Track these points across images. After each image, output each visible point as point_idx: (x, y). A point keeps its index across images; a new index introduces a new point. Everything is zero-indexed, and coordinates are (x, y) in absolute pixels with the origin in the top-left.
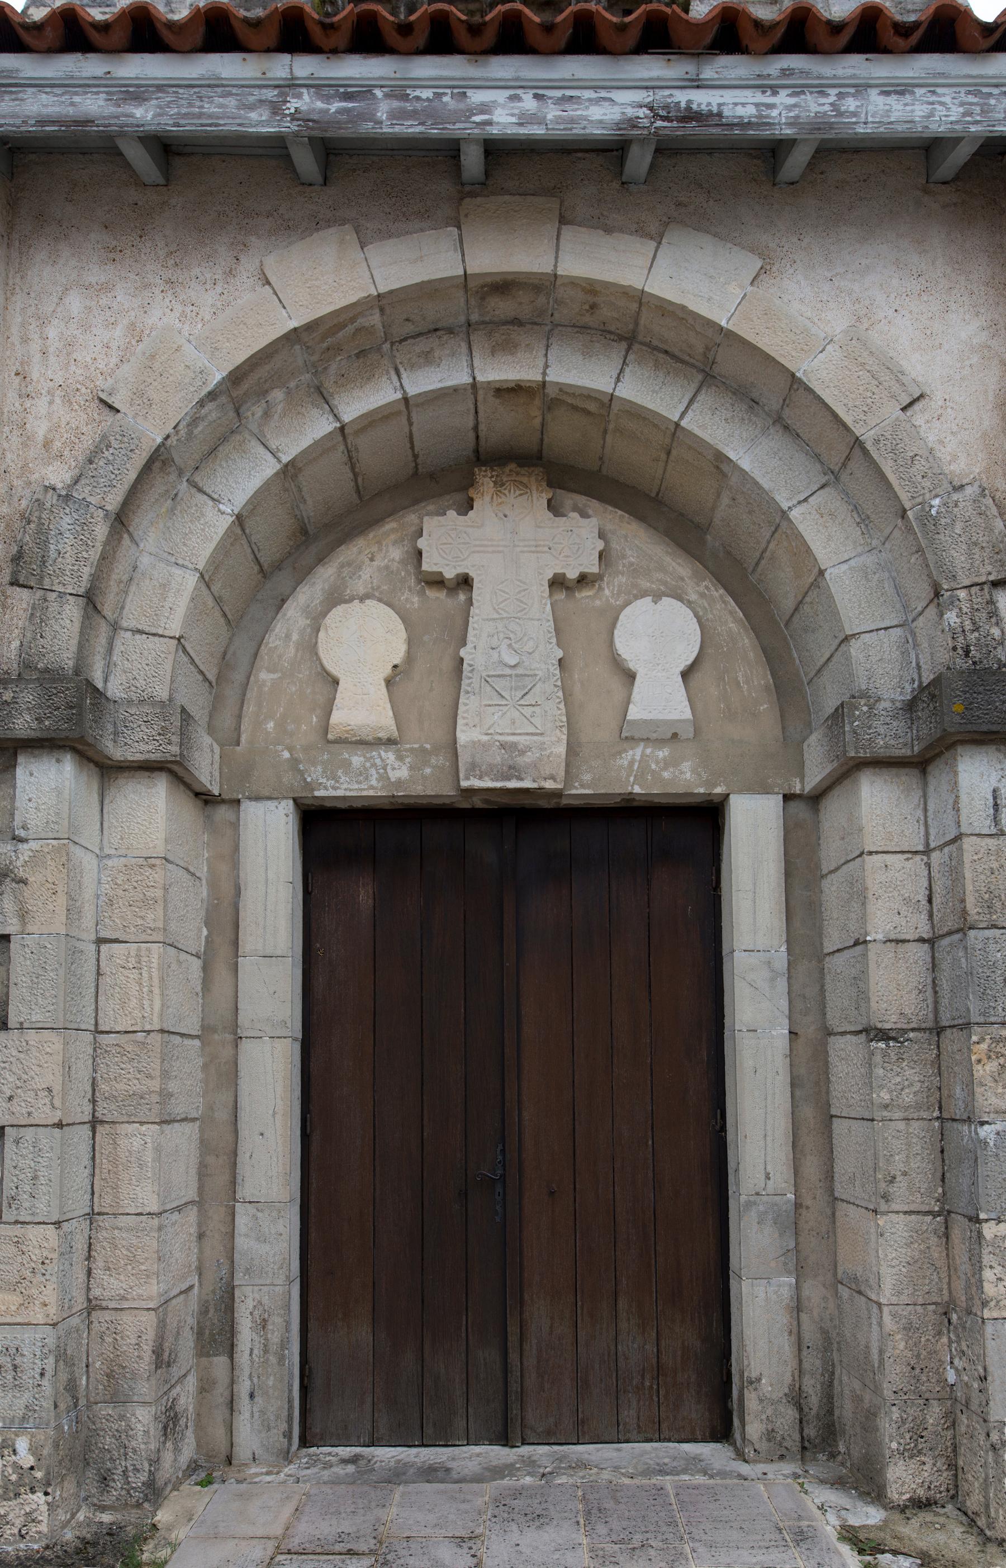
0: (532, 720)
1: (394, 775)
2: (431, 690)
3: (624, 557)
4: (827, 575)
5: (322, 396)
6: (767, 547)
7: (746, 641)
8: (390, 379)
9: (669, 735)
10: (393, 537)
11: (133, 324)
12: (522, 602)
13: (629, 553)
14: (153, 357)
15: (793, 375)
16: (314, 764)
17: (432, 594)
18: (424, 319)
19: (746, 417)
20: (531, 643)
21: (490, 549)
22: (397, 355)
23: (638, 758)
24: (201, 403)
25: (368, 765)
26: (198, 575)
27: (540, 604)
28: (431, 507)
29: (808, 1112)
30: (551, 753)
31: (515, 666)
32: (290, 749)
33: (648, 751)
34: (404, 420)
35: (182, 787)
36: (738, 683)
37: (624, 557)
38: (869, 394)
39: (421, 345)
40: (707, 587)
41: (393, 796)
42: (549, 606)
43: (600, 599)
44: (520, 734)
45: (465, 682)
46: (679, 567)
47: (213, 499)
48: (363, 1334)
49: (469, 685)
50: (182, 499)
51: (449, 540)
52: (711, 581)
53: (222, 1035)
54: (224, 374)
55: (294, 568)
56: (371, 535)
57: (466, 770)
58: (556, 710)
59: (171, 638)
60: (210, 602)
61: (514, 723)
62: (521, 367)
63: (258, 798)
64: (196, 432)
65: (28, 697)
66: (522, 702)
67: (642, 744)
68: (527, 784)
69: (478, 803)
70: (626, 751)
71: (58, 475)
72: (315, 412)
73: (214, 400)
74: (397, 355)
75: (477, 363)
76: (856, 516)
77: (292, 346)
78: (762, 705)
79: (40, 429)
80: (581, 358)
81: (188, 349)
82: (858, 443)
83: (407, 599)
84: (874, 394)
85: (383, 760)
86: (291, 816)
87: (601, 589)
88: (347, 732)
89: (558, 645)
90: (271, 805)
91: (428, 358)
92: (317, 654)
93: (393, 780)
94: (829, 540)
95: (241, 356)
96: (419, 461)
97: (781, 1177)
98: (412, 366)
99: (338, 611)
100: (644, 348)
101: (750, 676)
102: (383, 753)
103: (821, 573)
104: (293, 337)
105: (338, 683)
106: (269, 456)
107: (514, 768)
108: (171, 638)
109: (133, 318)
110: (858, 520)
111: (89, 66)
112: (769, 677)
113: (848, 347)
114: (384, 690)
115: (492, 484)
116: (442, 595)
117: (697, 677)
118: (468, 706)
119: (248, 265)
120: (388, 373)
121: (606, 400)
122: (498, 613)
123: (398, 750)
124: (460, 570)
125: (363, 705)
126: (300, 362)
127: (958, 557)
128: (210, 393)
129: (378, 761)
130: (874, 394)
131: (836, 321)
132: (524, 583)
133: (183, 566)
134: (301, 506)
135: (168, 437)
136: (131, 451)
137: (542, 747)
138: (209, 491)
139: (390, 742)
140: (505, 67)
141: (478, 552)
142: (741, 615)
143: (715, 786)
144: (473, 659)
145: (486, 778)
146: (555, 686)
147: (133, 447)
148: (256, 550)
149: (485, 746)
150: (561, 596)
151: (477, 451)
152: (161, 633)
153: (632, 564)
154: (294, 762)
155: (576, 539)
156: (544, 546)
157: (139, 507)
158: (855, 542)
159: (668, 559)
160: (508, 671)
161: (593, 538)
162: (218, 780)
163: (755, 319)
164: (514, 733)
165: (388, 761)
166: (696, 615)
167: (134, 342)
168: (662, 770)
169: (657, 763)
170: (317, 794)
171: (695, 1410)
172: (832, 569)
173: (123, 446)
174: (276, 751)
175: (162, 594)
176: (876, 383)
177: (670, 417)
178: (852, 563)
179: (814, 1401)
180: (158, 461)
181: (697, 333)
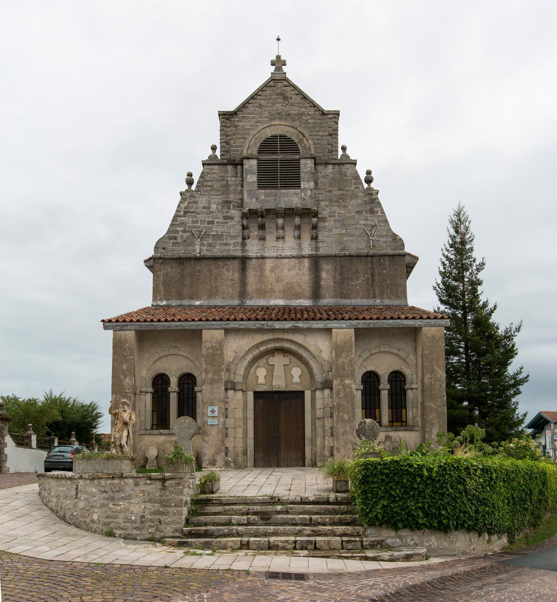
7: (307, 372)
29: (313, 428)
46: (299, 363)
48: (262, 454)
53: (245, 419)
58: (284, 381)
65: (229, 384)
71: (231, 360)
79: (229, 355)
91: (269, 343)
97: (310, 435)
101: (307, 376)
102: (345, 568)
111: (237, 322)
118: (274, 380)
119: (250, 336)
125: (261, 380)
127: (325, 369)
131: (313, 343)
140: (277, 322)
155: (286, 360)
164: (279, 384)
171: (301, 463)
179: (313, 461)
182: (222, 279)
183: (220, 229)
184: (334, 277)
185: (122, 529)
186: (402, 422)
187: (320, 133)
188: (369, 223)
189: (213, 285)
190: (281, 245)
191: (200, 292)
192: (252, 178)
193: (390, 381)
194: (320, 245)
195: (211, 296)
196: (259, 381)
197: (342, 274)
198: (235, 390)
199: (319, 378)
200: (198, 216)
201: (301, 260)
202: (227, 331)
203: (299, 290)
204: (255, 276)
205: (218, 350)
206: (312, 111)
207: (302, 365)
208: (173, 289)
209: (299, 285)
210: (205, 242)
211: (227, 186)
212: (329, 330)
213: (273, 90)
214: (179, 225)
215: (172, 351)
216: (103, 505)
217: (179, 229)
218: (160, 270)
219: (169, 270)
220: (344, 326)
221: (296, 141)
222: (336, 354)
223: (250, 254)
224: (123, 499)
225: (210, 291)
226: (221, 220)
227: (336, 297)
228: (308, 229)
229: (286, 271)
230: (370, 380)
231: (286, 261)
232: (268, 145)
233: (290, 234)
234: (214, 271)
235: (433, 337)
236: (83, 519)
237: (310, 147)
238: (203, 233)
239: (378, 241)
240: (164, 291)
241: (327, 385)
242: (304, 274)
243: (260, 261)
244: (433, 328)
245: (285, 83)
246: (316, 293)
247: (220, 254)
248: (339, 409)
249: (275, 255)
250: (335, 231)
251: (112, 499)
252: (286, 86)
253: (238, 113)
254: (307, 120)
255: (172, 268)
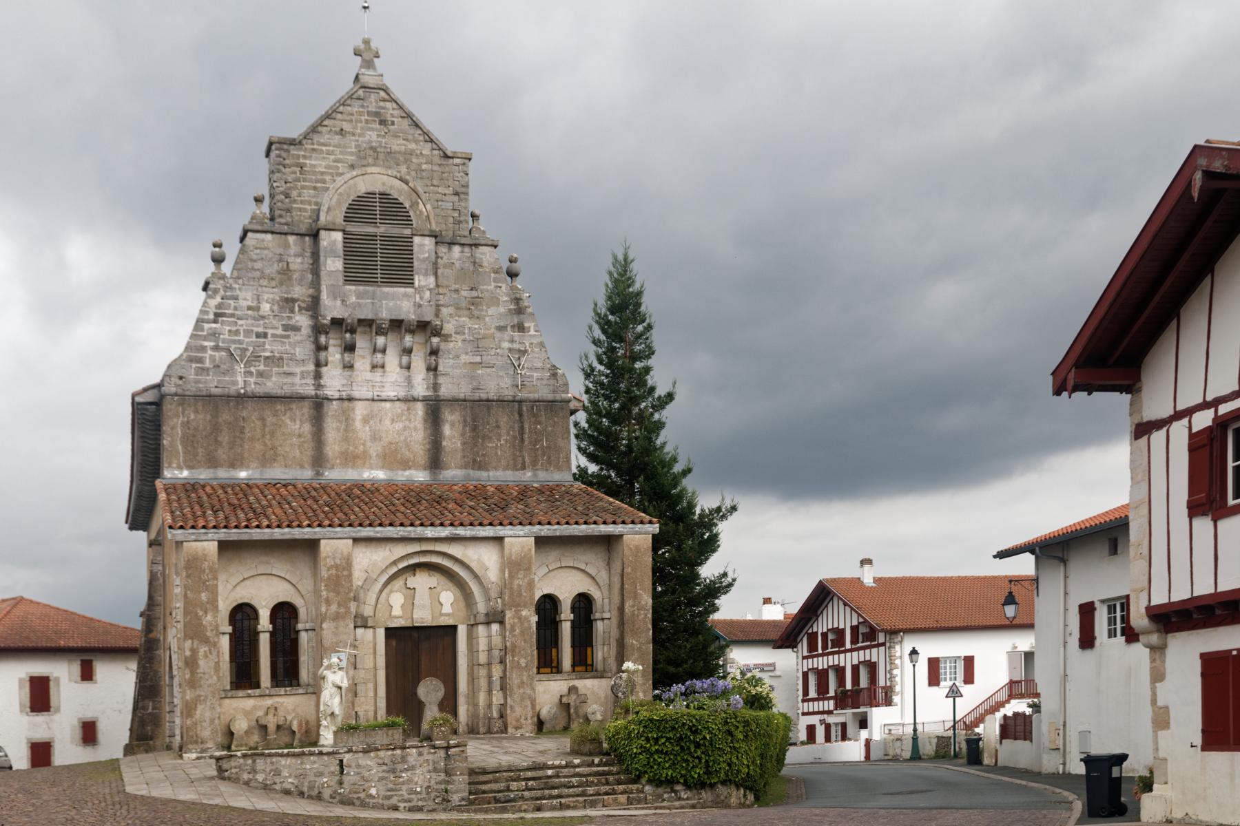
27: (427, 592)
46: (450, 585)
71: (360, 583)
101: (462, 604)
125: (397, 611)
164: (423, 616)
182: (284, 434)
183: (277, 348)
184: (463, 435)
185: (406, 801)
186: (586, 665)
187: (440, 190)
188: (516, 346)
189: (269, 443)
190: (378, 379)
191: (246, 455)
192: (333, 265)
193: (573, 609)
194: (441, 380)
195: (267, 460)
196: (395, 613)
197: (474, 429)
198: (365, 627)
199: (482, 607)
200: (240, 322)
201: (411, 404)
202: (356, 540)
203: (408, 455)
204: (338, 429)
205: (344, 569)
206: (426, 149)
207: (454, 588)
208: (200, 450)
209: (407, 446)
210: (252, 369)
211: (286, 272)
212: (499, 540)
213: (362, 106)
214: (205, 338)
215: (261, 570)
216: (381, 779)
217: (206, 343)
218: (177, 416)
219: (192, 416)
220: (521, 533)
221: (407, 205)
222: (510, 573)
223: (330, 392)
224: (406, 770)
225: (264, 455)
226: (280, 332)
227: (465, 467)
228: (421, 354)
229: (387, 422)
230: (548, 606)
231: (388, 405)
232: (359, 209)
233: (392, 359)
234: (270, 419)
235: (637, 548)
236: (356, 796)
237: (428, 216)
238: (248, 354)
239: (530, 377)
240: (184, 453)
241: (495, 617)
242: (415, 429)
243: (346, 403)
244: (637, 536)
245: (382, 94)
246: (435, 461)
247: (279, 392)
248: (513, 651)
249: (369, 395)
250: (465, 358)
251: (393, 771)
252: (384, 100)
253: (304, 142)
254: (420, 164)
255: (196, 412)
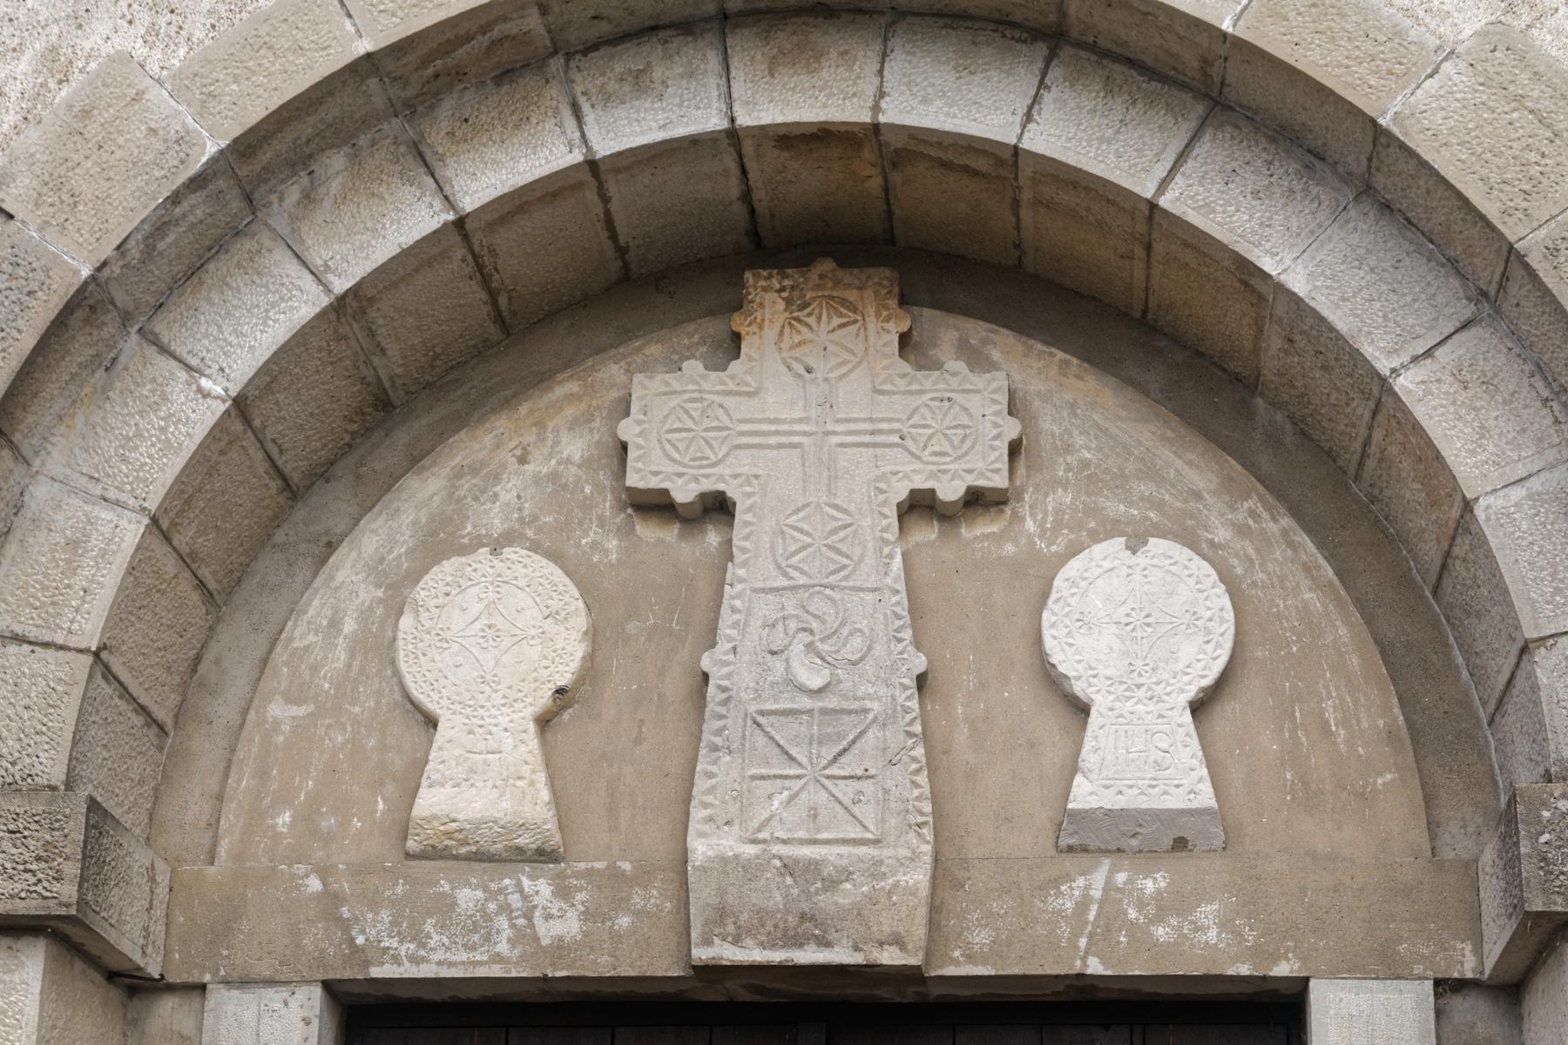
0: (856, 810)
1: (547, 931)
2: (638, 741)
3: (1068, 449)
4: (1479, 511)
5: (423, 159)
6: (1370, 436)
8: (560, 125)
9: (1168, 842)
10: (570, 412)
11: (54, 50)
12: (839, 552)
13: (1080, 440)
14: (87, 113)
15: (1373, 122)
16: (374, 906)
17: (650, 532)
18: (632, 13)
19: (1298, 187)
20: (857, 641)
21: (772, 440)
22: (578, 78)
23: (1097, 894)
24: (175, 198)
25: (492, 907)
26: (146, 521)
27: (881, 559)
28: (654, 350)
30: (896, 884)
31: (821, 691)
32: (324, 872)
33: (1121, 878)
34: (591, 196)
35: (79, 965)
36: (1326, 723)
37: (1068, 449)
38: (1533, 157)
39: (627, 60)
40: (1252, 513)
41: (545, 979)
42: (898, 558)
43: (1015, 542)
44: (828, 842)
45: (710, 725)
46: (1192, 471)
47: (189, 367)
49: (719, 732)
50: (126, 369)
51: (686, 411)
52: (1261, 499)
54: (223, 144)
55: (358, 477)
56: (523, 409)
57: (706, 924)
58: (909, 787)
59: (80, 651)
60: (170, 566)
61: (815, 816)
62: (829, 96)
63: (245, 982)
64: (161, 246)
66: (834, 770)
67: (1106, 863)
68: (840, 955)
69: (737, 990)
70: (1069, 878)
72: (406, 193)
73: (201, 187)
74: (578, 78)
75: (738, 89)
76: (1540, 384)
77: (363, 81)
78: (1380, 774)
80: (952, 76)
81: (159, 96)
82: (1512, 256)
83: (594, 544)
84: (1543, 155)
85: (525, 898)
86: (315, 1023)
87: (1017, 518)
88: (449, 835)
89: (918, 644)
90: (274, 997)
92: (393, 663)
93: (545, 942)
94: (1482, 436)
95: (255, 113)
96: (631, 256)
98: (607, 99)
99: (447, 569)
100: (1083, 53)
101: (1351, 707)
102: (526, 882)
103: (1468, 506)
104: (368, 64)
105: (435, 726)
106: (307, 281)
107: (812, 918)
108: (80, 651)
109: (54, 38)
110: (1546, 393)
112: (1397, 710)
113: (1488, 65)
114: (533, 743)
115: (781, 305)
116: (669, 534)
117: (1226, 714)
118: (718, 775)
120: (557, 111)
121: (1007, 155)
122: (786, 575)
123: (561, 876)
124: (707, 486)
125: (485, 776)
126: (379, 101)
128: (192, 180)
129: (515, 900)
130: (1543, 155)
132: (845, 511)
133: (117, 503)
134: (376, 360)
135: (105, 264)
136: (29, 293)
137: (875, 870)
138: (181, 351)
139: (543, 855)
141: (748, 446)
142: (1330, 572)
143: (1275, 959)
144: (729, 676)
145: (749, 942)
146: (910, 734)
147: (34, 286)
148: (274, 451)
149: (751, 870)
150: (926, 533)
151: (754, 232)
152: (60, 640)
153: (1085, 464)
154: (331, 899)
156: (891, 432)
157: (35, 395)
158: (1540, 440)
159: (1166, 453)
160: (805, 702)
161: (996, 414)
162: (160, 942)
163: (1292, 15)
165: (536, 900)
166: (1226, 577)
167: (52, 84)
168: (1151, 922)
169: (1141, 906)
170: (376, 972)
172: (1491, 499)
173: (14, 284)
174: (293, 877)
175: (68, 561)
176: (1549, 134)
177: (1137, 190)
178: (1535, 484)
180: (85, 308)
181: (1181, 38)
